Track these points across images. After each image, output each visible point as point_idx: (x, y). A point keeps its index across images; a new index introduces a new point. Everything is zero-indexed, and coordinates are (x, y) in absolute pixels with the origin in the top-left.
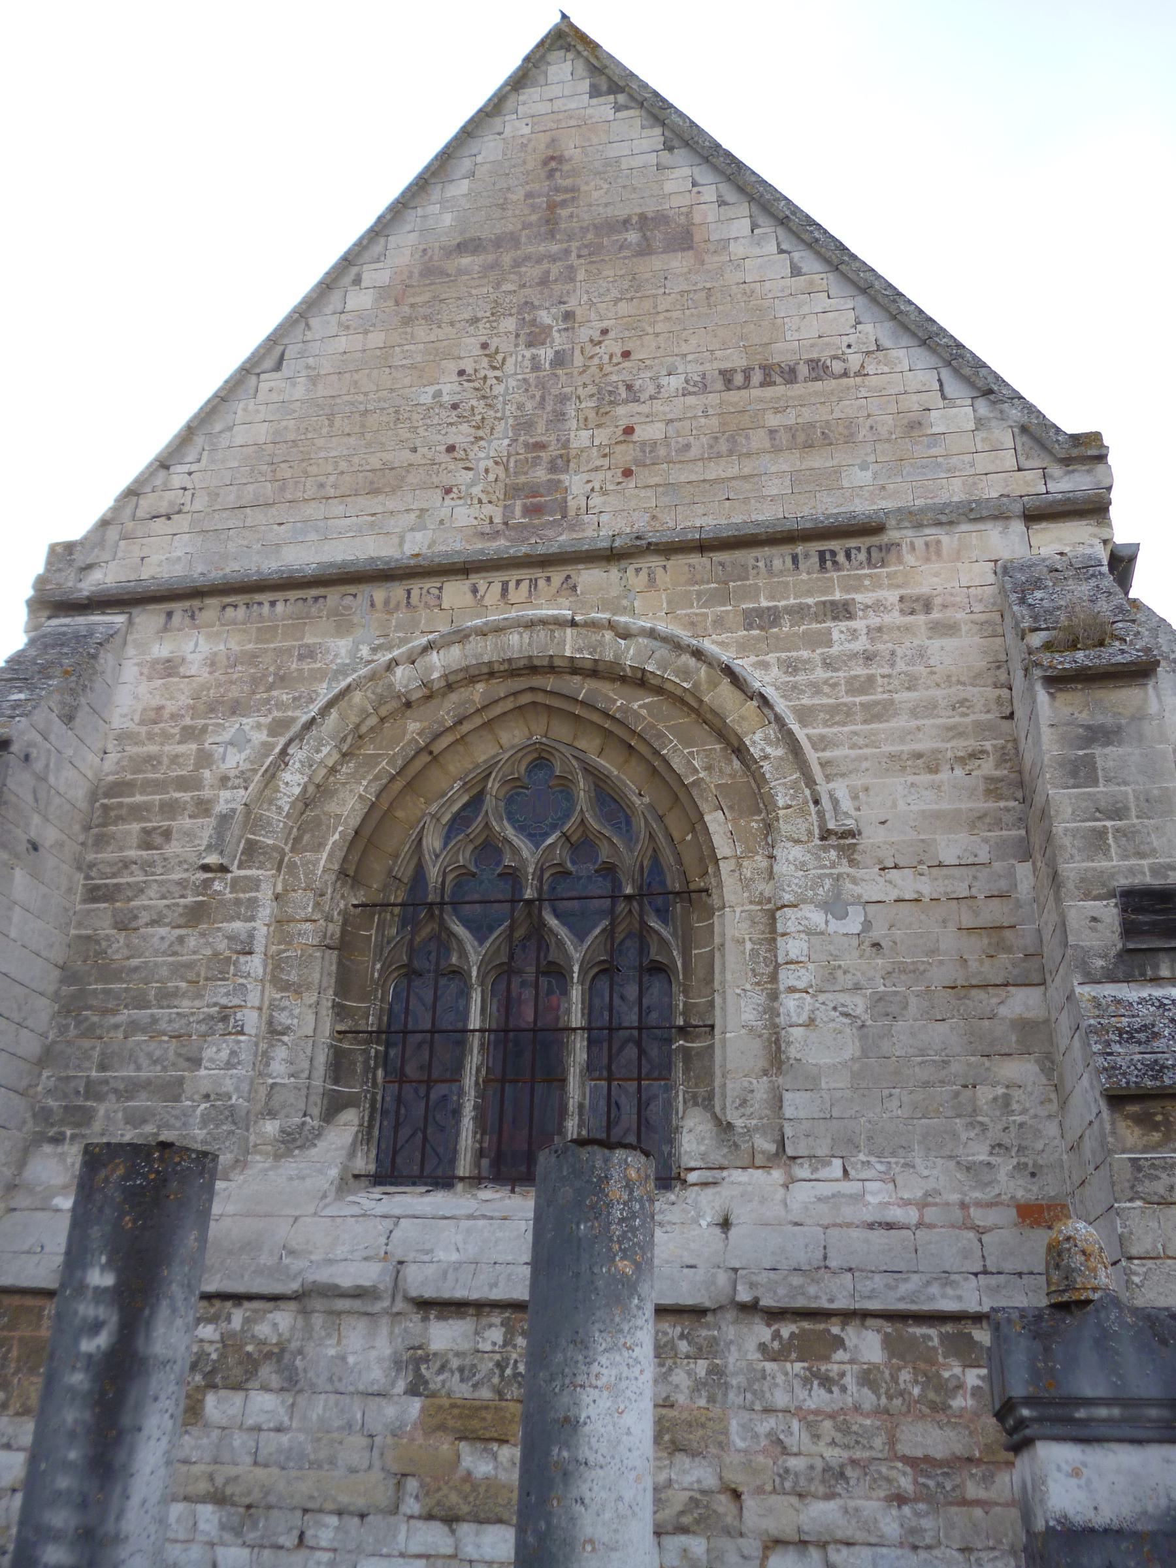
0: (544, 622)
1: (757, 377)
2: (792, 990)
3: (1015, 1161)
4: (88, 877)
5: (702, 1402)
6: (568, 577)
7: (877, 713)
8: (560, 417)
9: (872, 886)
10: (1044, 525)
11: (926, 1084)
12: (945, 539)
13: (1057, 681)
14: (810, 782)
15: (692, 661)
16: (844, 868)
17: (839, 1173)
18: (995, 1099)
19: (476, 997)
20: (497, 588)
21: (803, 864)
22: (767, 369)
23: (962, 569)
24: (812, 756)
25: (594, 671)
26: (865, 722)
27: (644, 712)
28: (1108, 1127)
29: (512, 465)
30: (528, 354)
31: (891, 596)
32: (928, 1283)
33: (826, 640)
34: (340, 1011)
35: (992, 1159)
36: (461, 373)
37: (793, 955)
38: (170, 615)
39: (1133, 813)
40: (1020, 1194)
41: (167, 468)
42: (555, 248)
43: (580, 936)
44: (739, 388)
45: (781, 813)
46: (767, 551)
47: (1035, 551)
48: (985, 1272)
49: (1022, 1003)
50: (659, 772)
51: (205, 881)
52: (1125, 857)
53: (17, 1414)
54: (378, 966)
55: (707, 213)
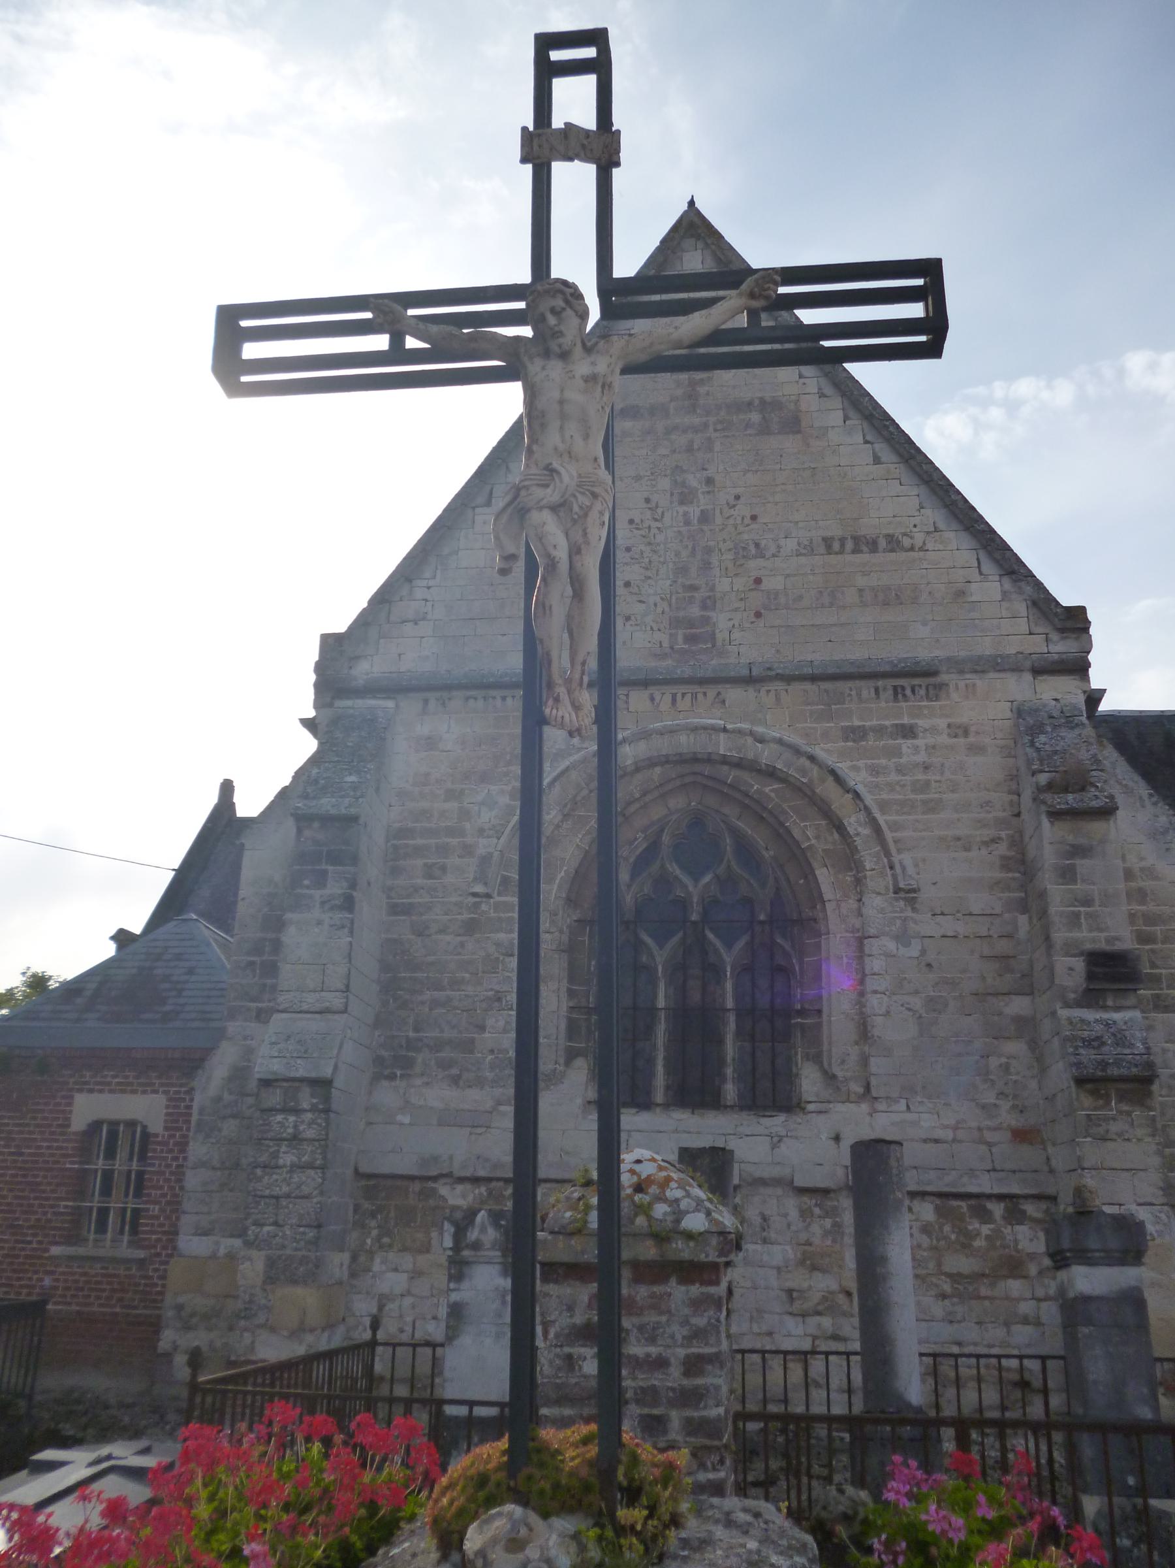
0: (705, 728)
1: (849, 545)
2: (875, 992)
3: (1011, 1103)
4: (389, 897)
5: (829, 1242)
6: (719, 694)
7: (932, 807)
8: (706, 566)
9: (927, 925)
10: (1045, 677)
11: (959, 1055)
12: (979, 683)
13: (1056, 815)
14: (888, 854)
15: (807, 763)
16: (909, 913)
17: (904, 1108)
18: (1001, 1065)
19: (662, 986)
20: (668, 698)
21: (883, 909)
22: (856, 539)
23: (990, 705)
24: (889, 836)
25: (739, 764)
26: (923, 813)
27: (773, 795)
28: (1074, 1096)
29: (674, 601)
30: (682, 509)
31: (942, 723)
32: (962, 1176)
33: (896, 752)
34: (571, 993)
35: (997, 1102)
36: (631, 521)
37: (876, 970)
38: (426, 701)
39: (1097, 903)
40: (1013, 1123)
41: (410, 581)
42: (697, 421)
43: (729, 946)
44: (836, 553)
45: (868, 873)
46: (858, 683)
47: (1038, 696)
48: (994, 1170)
49: (1019, 1006)
50: (782, 835)
51: (475, 903)
52: (1090, 931)
53: (400, 1251)
54: (593, 963)
55: (811, 403)
